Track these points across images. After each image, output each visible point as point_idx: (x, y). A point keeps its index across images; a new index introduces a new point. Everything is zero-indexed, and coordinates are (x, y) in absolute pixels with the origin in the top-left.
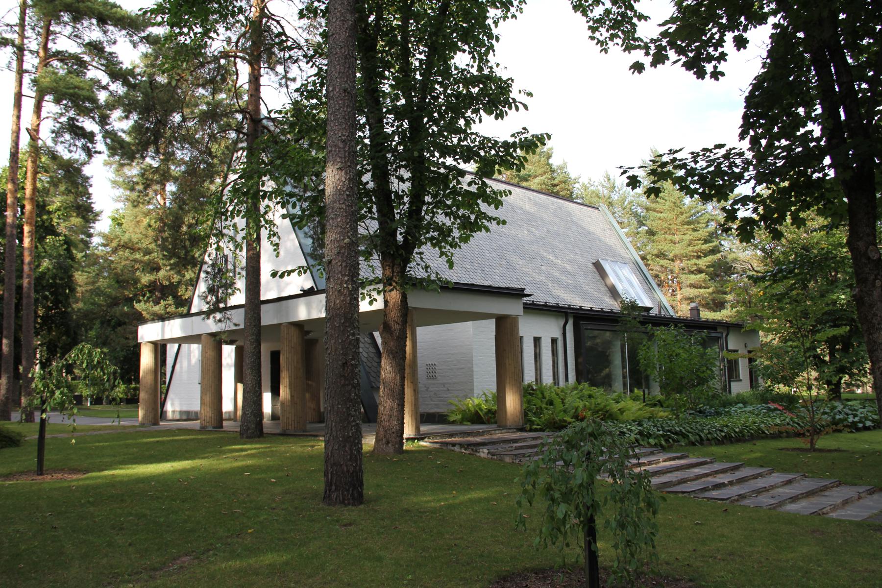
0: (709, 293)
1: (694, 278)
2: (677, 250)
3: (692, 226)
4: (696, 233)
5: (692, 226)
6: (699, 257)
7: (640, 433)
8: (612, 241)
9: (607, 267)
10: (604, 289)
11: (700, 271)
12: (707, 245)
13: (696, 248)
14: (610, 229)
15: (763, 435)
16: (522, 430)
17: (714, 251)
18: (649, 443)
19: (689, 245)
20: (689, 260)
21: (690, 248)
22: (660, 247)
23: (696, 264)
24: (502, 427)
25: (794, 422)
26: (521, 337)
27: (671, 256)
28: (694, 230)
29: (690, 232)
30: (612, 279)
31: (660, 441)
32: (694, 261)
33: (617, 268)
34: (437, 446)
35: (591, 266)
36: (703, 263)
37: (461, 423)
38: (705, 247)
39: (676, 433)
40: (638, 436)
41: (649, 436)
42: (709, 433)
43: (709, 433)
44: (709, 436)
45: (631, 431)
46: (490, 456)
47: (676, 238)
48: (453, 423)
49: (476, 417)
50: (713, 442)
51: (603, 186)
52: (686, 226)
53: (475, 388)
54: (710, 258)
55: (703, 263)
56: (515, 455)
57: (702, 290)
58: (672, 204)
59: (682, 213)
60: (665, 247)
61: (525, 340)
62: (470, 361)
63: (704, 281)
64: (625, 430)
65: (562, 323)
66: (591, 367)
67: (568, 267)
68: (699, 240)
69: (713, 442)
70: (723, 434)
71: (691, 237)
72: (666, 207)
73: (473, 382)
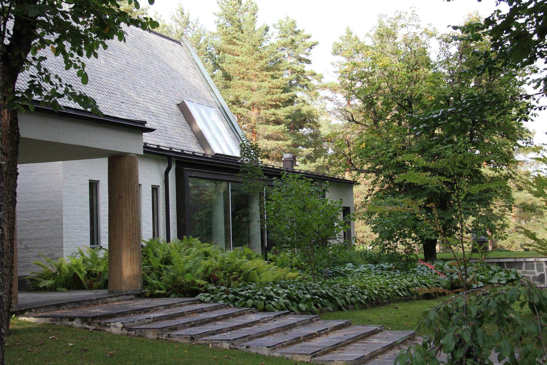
0: (289, 146)
1: (272, 129)
2: (256, 97)
3: (272, 73)
4: (275, 81)
5: (272, 73)
6: (277, 107)
7: (289, 297)
8: (196, 81)
9: (193, 108)
10: (190, 134)
11: (277, 122)
12: (287, 94)
13: (275, 97)
14: (194, 68)
15: (398, 298)
16: (140, 296)
17: (290, 102)
18: (299, 309)
19: (268, 93)
20: (268, 109)
21: (269, 97)
22: (236, 93)
23: (274, 114)
24: (117, 294)
25: (421, 283)
26: (140, 185)
27: (248, 103)
28: (273, 77)
29: (269, 79)
30: (200, 124)
31: (310, 306)
32: (273, 110)
33: (203, 111)
34: (47, 321)
35: (175, 107)
36: (282, 113)
37: (52, 289)
38: (284, 96)
39: (323, 296)
40: (287, 301)
41: (298, 300)
42: (353, 296)
43: (353, 296)
44: (353, 299)
45: (278, 294)
46: (125, 332)
47: (254, 85)
48: (45, 289)
49: (73, 282)
50: (357, 306)
51: (177, 21)
52: (265, 73)
53: (65, 245)
54: (289, 108)
55: (282, 113)
56: (161, 329)
57: (280, 142)
58: (251, 47)
59: (261, 58)
60: (242, 93)
61: (143, 187)
62: (60, 212)
63: (284, 132)
64: (272, 293)
65: (164, 168)
66: (191, 221)
67: (152, 108)
68: (278, 88)
69: (357, 306)
70: (365, 297)
71: (270, 85)
72: (244, 49)
73: (61, 238)
